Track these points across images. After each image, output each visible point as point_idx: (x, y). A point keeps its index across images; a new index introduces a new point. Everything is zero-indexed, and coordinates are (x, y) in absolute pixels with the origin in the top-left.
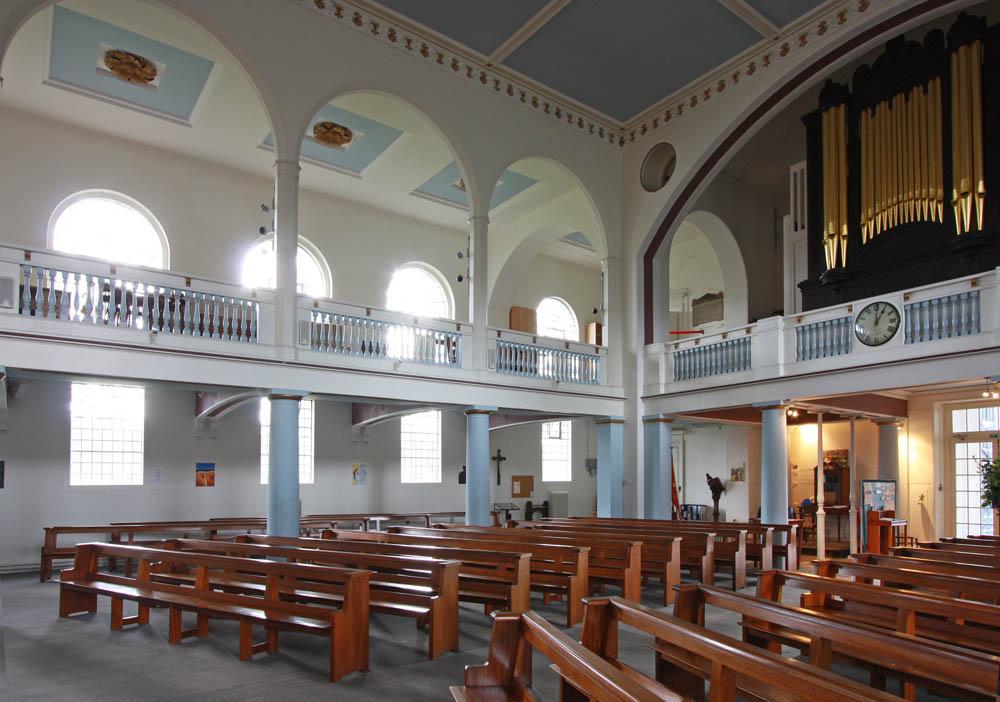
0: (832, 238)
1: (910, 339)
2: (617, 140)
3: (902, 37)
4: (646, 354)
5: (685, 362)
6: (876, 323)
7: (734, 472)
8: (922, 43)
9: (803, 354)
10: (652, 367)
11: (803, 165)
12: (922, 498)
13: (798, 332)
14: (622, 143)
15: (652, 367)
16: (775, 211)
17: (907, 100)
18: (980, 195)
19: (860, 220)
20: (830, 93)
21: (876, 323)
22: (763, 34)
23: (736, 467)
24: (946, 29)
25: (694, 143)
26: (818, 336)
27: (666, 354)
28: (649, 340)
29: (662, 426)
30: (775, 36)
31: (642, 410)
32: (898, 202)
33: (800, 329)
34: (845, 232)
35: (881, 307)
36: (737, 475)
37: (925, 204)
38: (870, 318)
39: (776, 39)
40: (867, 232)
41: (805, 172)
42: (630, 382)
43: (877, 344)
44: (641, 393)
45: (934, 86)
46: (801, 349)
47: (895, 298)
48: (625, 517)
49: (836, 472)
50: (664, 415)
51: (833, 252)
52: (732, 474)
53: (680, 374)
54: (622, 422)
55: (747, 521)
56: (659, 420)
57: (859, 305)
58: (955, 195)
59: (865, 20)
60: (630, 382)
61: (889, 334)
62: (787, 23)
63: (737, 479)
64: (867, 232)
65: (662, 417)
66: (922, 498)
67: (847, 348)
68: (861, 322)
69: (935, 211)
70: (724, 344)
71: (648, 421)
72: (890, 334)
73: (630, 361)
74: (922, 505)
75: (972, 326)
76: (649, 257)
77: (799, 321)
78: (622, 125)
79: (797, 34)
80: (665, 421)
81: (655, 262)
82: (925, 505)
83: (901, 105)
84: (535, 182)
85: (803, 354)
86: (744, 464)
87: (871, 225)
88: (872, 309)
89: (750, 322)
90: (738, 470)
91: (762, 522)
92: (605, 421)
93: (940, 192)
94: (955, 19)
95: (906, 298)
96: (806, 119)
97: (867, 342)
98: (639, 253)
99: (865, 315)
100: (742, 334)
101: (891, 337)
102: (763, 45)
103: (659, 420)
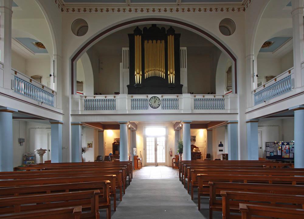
0: (138, 74)
1: (133, 108)
2: (241, 10)
3: (155, 25)
4: (72, 98)
5: (106, 103)
6: (155, 102)
7: (89, 144)
8: (148, 29)
9: (133, 108)
10: (76, 103)
11: (128, 49)
12: (140, 152)
13: (131, 101)
14: (244, 10)
15: (76, 103)
16: (99, 60)
17: (156, 43)
18: (141, 75)
19: (135, 73)
20: (137, 30)
21: (155, 102)
22: (126, 2)
23: (89, 143)
24: (167, 29)
25: (97, 25)
26: (109, 103)
27: (81, 99)
28: (72, 93)
29: (80, 126)
30: (129, 4)
31: (71, 120)
32: (154, 70)
33: (86, 100)
34: (141, 74)
35: (156, 98)
36: (90, 145)
37: (159, 72)
38: (153, 100)
39: (129, 5)
40: (146, 75)
41: (186, 50)
42: (66, 108)
43: (155, 108)
44: (70, 113)
45: (163, 42)
46: (132, 106)
47: (159, 96)
48: (60, 162)
49: (116, 146)
50: (81, 122)
51: (138, 78)
52: (88, 145)
53: (87, 108)
54: (62, 123)
55: (258, 159)
56: (78, 124)
57: (150, 96)
58: (169, 73)
59: (153, 15)
60: (66, 108)
61: (158, 106)
62: (134, 2)
63: (90, 147)
64: (146, 75)
65: (80, 123)
66: (140, 152)
67: (147, 108)
68: (150, 101)
69: (163, 75)
70: (105, 100)
71: (73, 124)
72: (152, 106)
73: (66, 100)
74: (140, 154)
75: (177, 107)
76: (73, 59)
77: (132, 97)
78: (65, 3)
79: (89, 7)
80: (81, 125)
81: (74, 62)
82: (141, 154)
83: (159, 43)
84: (17, 6)
85: (195, 107)
86: (92, 142)
87: (147, 73)
88: (154, 98)
89: (94, 94)
90: (90, 144)
91: (120, 161)
92: (57, 123)
93: (164, 70)
94: (136, 28)
95: (162, 97)
96: (130, 35)
97: (152, 107)
98: (70, 58)
99: (152, 99)
100: (221, 97)
101: (159, 107)
102: (124, 5)
103: (78, 124)
